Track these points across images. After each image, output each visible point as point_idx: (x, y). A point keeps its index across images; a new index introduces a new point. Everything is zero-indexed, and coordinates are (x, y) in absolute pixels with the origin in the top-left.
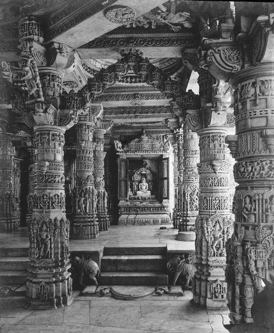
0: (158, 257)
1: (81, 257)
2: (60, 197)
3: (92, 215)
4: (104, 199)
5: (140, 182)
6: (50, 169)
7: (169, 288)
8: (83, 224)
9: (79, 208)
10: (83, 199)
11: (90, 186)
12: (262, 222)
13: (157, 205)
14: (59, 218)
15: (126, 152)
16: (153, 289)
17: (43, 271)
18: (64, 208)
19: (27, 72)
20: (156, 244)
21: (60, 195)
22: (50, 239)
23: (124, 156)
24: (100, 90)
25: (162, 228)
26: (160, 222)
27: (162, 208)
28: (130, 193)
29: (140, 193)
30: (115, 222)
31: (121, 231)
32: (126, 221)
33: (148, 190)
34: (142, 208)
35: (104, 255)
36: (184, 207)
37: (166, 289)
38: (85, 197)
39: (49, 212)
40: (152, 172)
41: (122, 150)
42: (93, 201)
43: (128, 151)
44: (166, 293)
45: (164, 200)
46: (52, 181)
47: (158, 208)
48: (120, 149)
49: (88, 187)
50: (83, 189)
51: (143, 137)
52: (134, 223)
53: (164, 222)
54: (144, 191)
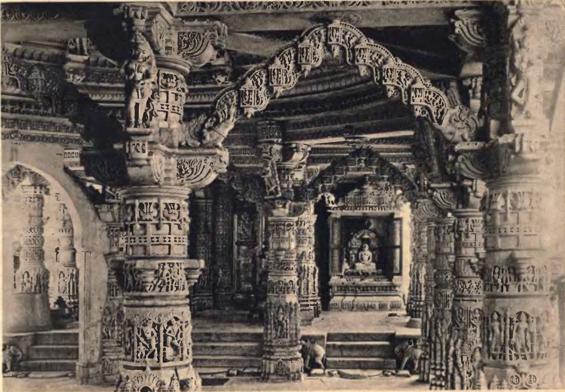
0: (386, 343)
5: (361, 249)
7: (397, 371)
13: (385, 282)
14: (293, 302)
15: (342, 208)
16: (381, 372)
17: (280, 349)
19: (268, 172)
20: (385, 330)
22: (286, 321)
23: (337, 214)
25: (391, 315)
26: (389, 307)
27: (392, 288)
28: (346, 266)
29: (360, 266)
30: (326, 306)
31: (330, 316)
32: (340, 306)
34: (363, 287)
36: (417, 290)
37: (394, 371)
39: (284, 297)
40: (377, 236)
41: (335, 205)
42: (308, 281)
44: (393, 374)
47: (386, 287)
49: (303, 265)
51: (365, 187)
52: (352, 308)
53: (395, 306)
54: (367, 263)
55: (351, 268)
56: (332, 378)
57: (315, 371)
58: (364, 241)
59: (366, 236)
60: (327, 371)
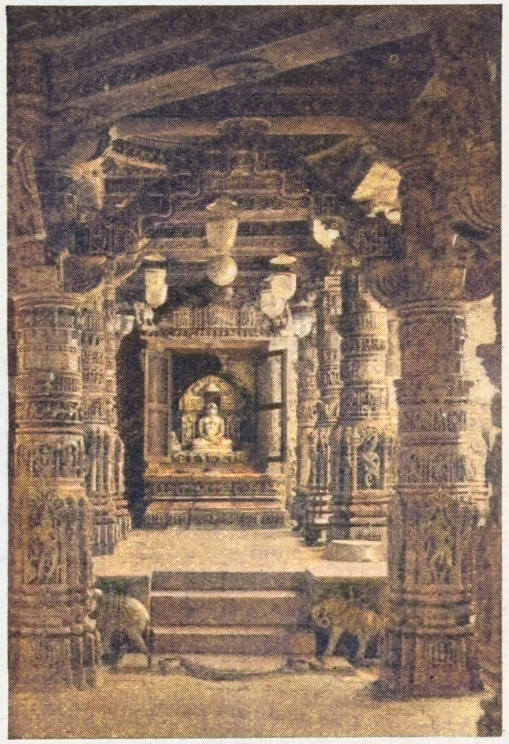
2: (76, 453)
3: (104, 497)
5: (203, 413)
12: (244, 229)
29: (202, 447)
33: (225, 436)
37: (313, 660)
41: (153, 328)
43: (171, 332)
44: (313, 667)
45: (270, 464)
48: (149, 324)
54: (214, 442)
55: (183, 449)
56: (167, 678)
57: (127, 659)
58: (208, 397)
59: (213, 388)
60: (156, 660)
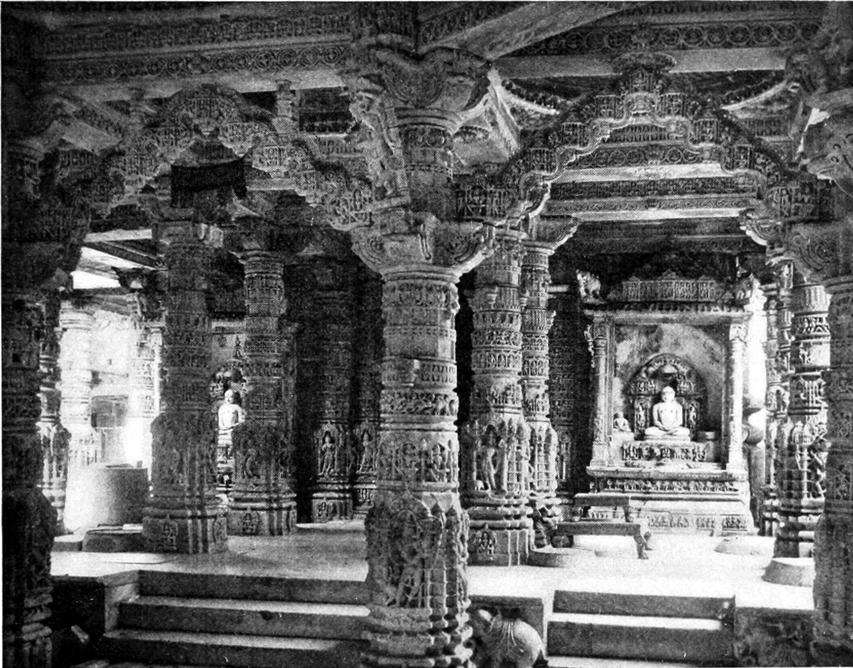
0: (712, 625)
1: (493, 613)
4: (547, 452)
5: (658, 398)
6: (423, 380)
8: (491, 522)
9: (479, 478)
10: (491, 452)
11: (512, 415)
18: (456, 479)
21: (445, 445)
24: (554, 168)
35: (556, 609)
38: (497, 447)
46: (427, 409)
50: (493, 424)
